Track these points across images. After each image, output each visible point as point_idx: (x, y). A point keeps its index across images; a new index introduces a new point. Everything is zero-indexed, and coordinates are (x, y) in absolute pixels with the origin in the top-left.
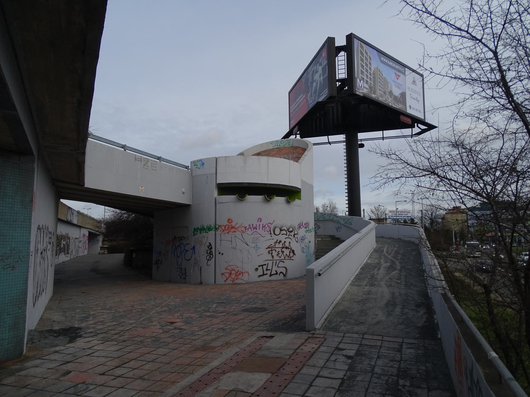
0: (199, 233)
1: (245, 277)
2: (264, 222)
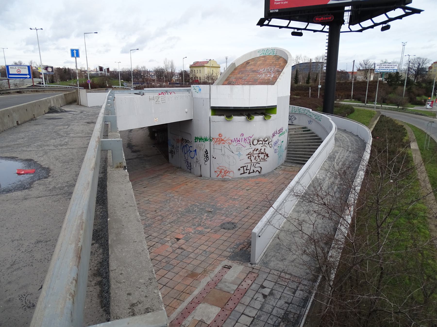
0: (198, 141)
1: (231, 175)
2: (245, 136)
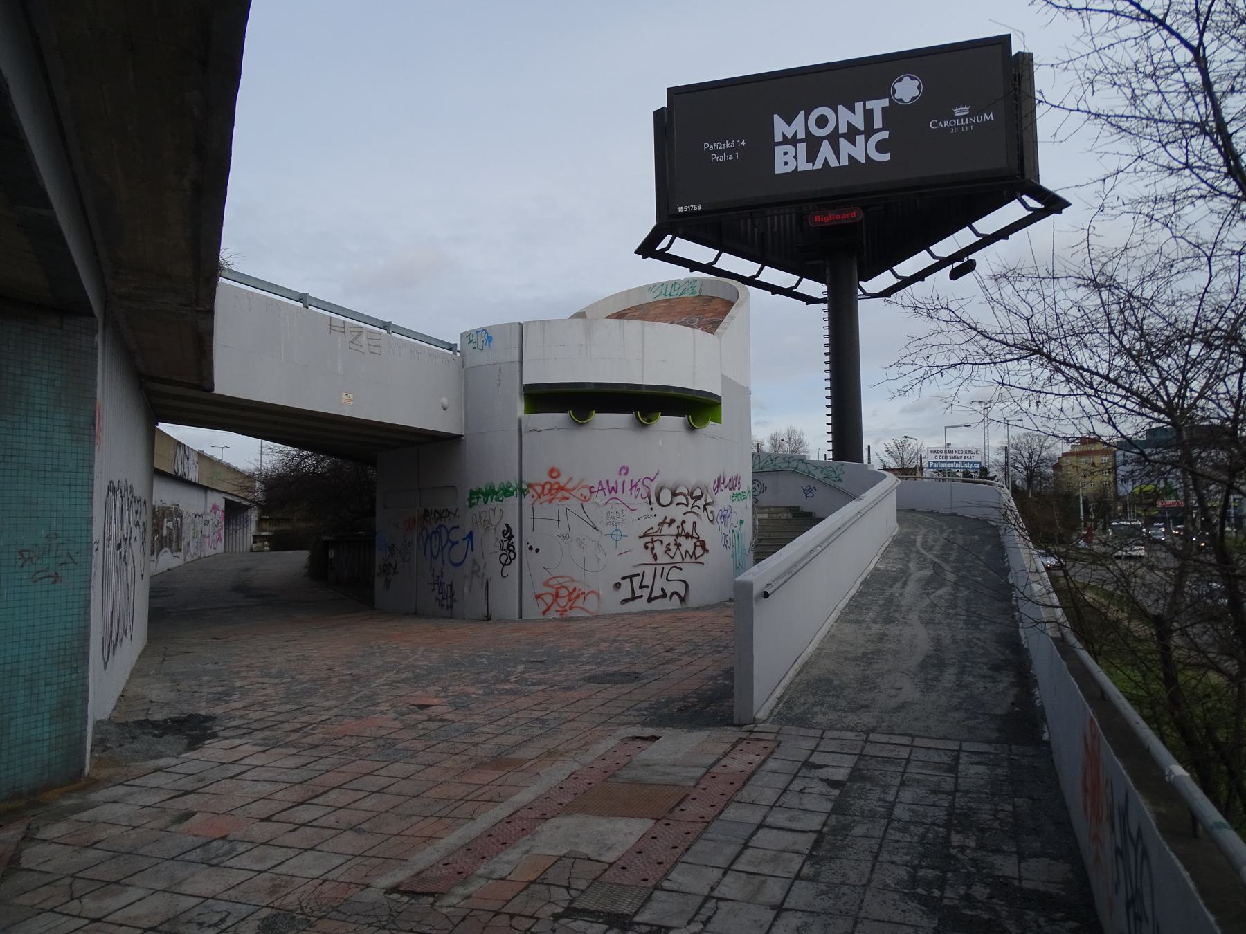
0: (481, 500)
2: (634, 476)
